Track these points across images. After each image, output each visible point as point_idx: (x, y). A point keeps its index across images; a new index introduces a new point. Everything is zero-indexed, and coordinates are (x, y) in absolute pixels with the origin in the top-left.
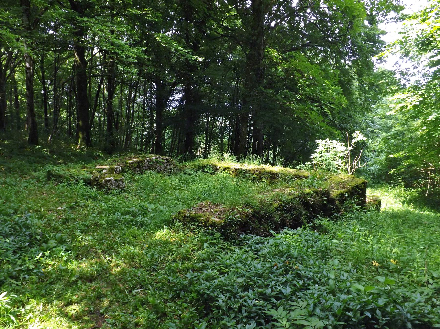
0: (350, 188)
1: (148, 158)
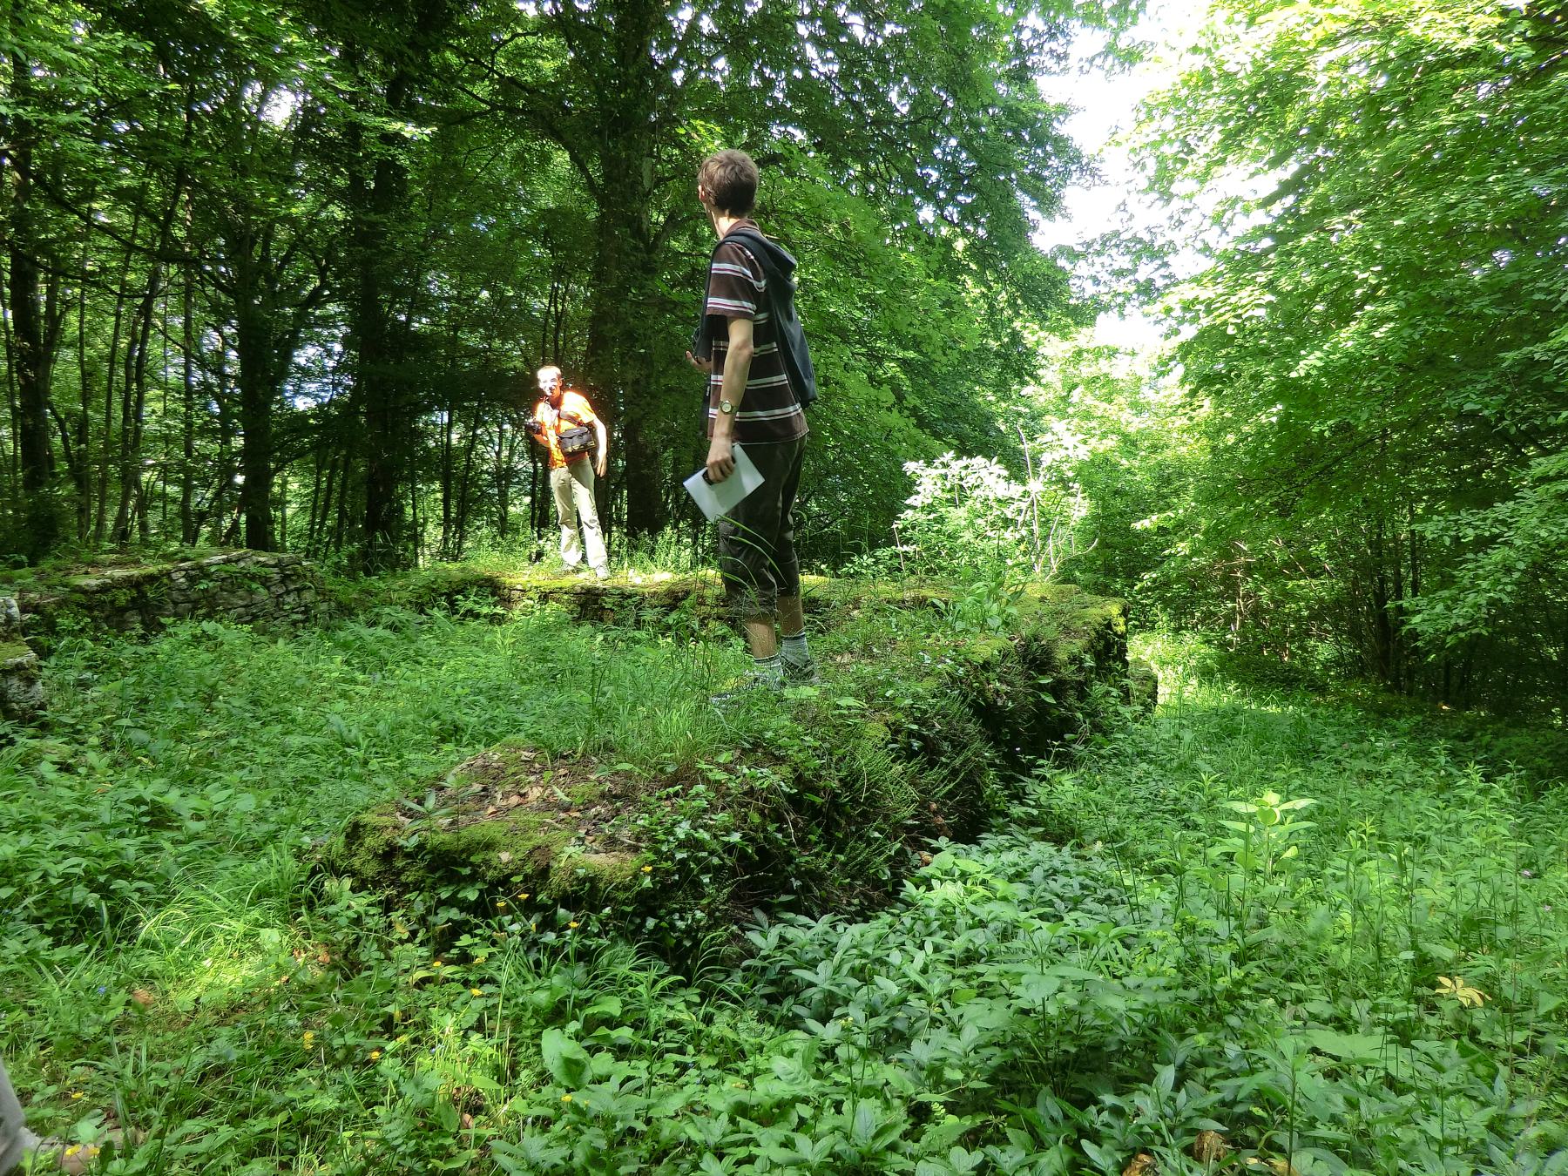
0: (1093, 634)
1: (184, 560)
